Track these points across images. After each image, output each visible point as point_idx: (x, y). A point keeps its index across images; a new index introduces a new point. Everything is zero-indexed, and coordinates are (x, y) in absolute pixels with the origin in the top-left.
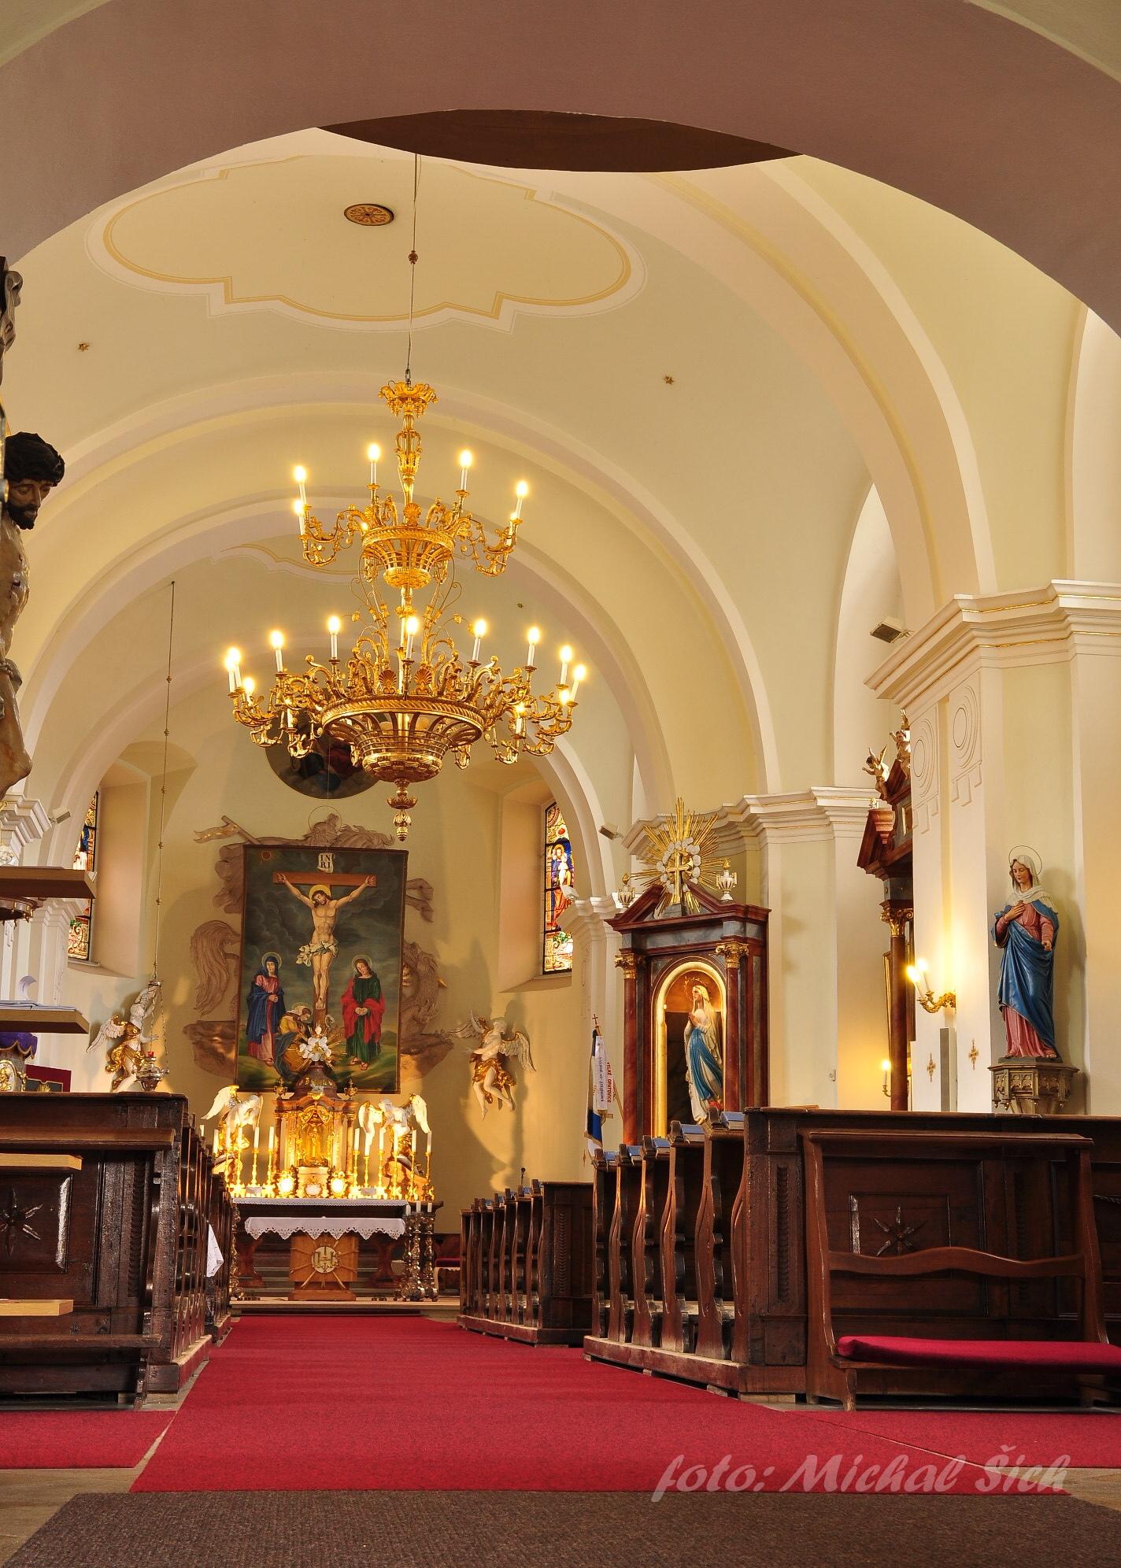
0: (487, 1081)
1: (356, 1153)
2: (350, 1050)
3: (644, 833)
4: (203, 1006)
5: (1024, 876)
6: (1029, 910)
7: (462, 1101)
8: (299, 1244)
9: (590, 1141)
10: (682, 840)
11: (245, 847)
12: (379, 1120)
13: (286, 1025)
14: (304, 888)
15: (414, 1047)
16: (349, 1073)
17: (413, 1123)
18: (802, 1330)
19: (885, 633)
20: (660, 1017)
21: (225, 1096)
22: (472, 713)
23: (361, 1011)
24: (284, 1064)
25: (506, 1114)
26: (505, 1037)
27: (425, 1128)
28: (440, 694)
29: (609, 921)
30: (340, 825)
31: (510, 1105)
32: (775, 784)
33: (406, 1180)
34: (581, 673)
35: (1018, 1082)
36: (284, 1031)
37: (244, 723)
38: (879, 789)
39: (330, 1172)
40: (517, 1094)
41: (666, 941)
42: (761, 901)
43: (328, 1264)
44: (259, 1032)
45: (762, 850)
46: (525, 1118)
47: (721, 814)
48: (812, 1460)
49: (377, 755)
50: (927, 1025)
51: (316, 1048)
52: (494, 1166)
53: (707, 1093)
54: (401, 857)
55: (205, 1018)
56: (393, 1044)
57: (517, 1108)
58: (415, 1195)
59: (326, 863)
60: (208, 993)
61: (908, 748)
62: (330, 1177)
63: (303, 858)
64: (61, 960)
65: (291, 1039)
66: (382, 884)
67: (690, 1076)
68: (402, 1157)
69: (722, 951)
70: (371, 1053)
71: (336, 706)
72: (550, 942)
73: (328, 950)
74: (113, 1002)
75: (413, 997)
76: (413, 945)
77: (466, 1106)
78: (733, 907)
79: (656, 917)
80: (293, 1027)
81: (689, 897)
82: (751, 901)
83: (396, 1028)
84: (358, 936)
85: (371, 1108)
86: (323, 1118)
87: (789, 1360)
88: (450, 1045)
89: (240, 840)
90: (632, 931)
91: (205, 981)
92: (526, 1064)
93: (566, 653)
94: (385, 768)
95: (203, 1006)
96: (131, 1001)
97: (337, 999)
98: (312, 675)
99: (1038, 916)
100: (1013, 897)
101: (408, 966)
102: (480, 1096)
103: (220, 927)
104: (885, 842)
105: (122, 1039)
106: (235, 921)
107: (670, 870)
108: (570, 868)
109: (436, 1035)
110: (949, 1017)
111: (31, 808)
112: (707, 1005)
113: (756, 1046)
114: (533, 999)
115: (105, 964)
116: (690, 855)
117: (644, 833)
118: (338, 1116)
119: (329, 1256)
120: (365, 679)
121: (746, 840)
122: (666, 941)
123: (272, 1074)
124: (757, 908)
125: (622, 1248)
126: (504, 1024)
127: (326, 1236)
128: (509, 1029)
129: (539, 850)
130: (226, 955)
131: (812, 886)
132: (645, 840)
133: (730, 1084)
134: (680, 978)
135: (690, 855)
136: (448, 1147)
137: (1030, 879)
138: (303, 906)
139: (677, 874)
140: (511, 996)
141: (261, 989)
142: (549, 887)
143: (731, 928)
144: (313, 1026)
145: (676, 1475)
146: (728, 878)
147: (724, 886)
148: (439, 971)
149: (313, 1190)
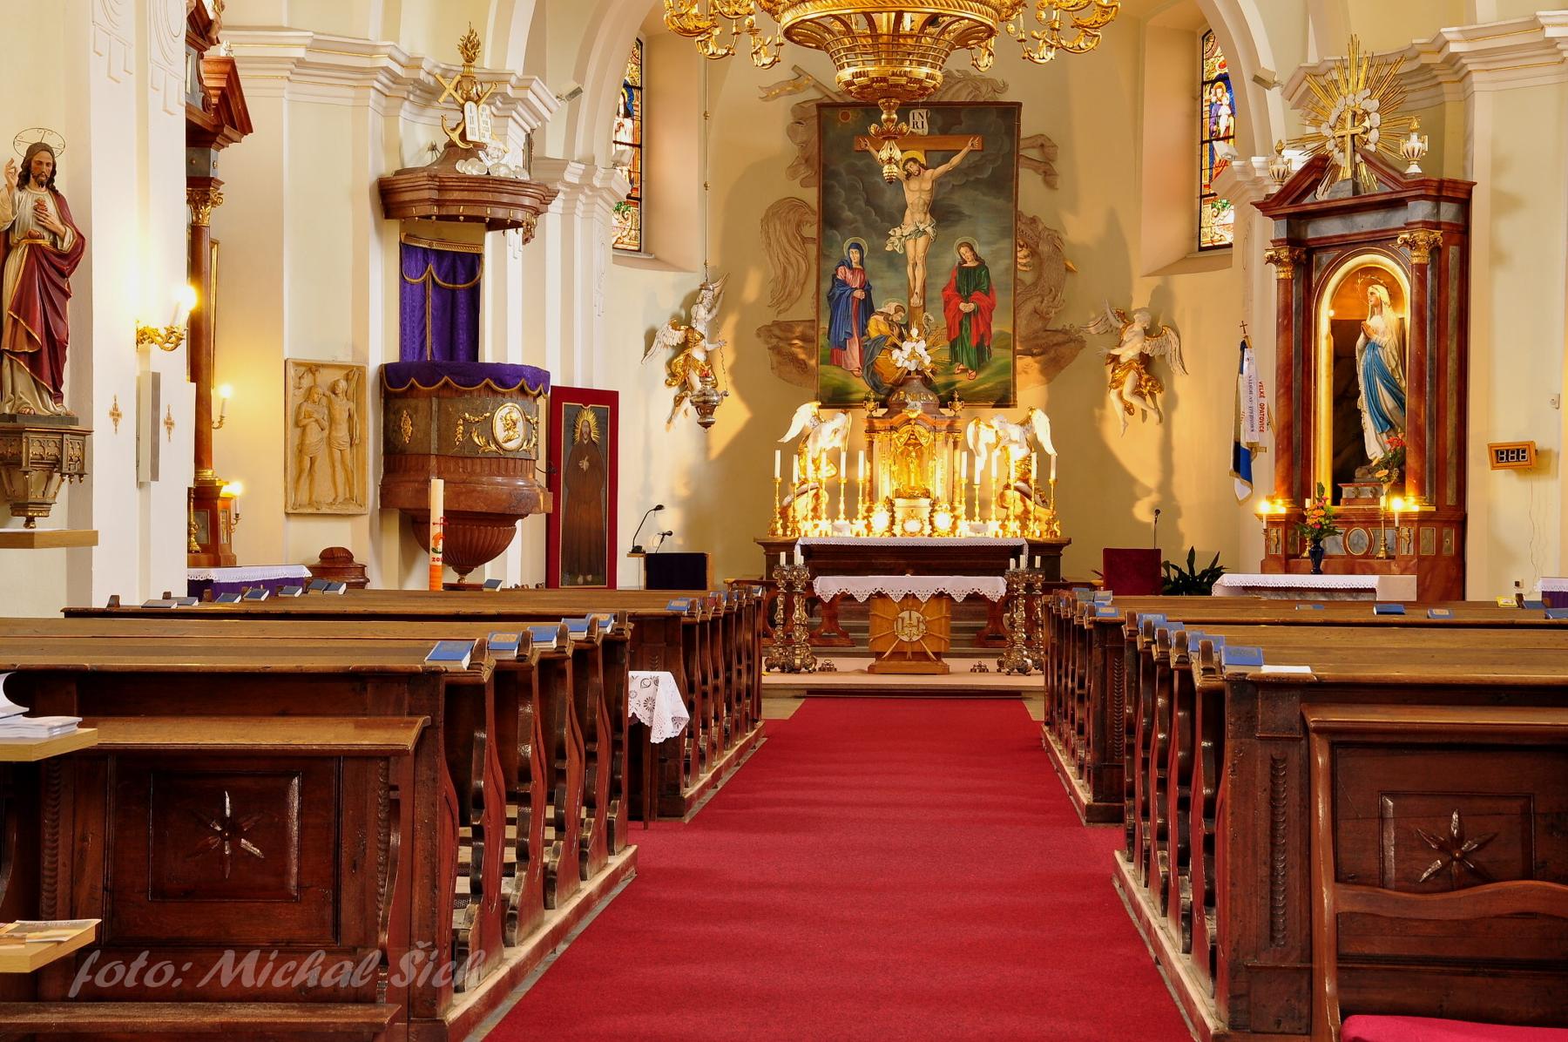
0: (1127, 387)
1: (964, 481)
2: (955, 357)
3: (1305, 85)
7: (1097, 411)
8: (879, 608)
9: (1237, 482)
10: (1356, 95)
11: (821, 106)
12: (993, 440)
13: (876, 326)
15: (1037, 346)
16: (953, 384)
17: (1034, 444)
18: (1305, 985)
20: (1324, 328)
21: (805, 414)
23: (966, 307)
24: (874, 374)
25: (1151, 428)
26: (1148, 333)
27: (1049, 449)
29: (1257, 205)
31: (1156, 417)
33: (1026, 511)
36: (874, 334)
39: (933, 505)
40: (1165, 403)
41: (1331, 228)
42: (1464, 169)
43: (914, 630)
44: (843, 336)
45: (1466, 100)
47: (1410, 54)
48: (229, 955)
51: (913, 354)
52: (1138, 491)
53: (1386, 423)
55: (781, 318)
56: (1006, 347)
57: (1165, 420)
58: (1037, 531)
60: (784, 288)
62: (933, 511)
64: (603, 255)
65: (882, 344)
67: (1363, 403)
69: (1406, 242)
72: (1207, 210)
73: (924, 232)
74: (672, 304)
75: (1035, 284)
76: (1034, 220)
77: (1102, 418)
78: (1421, 183)
80: (884, 328)
81: (1363, 169)
82: (1449, 173)
84: (960, 214)
85: (982, 426)
86: (923, 441)
87: (1285, 1027)
88: (1081, 343)
89: (814, 95)
90: (1289, 216)
91: (779, 272)
92: (1176, 367)
94: (863, 87)
95: (779, 303)
96: (691, 300)
97: (936, 294)
101: (1027, 245)
103: (796, 204)
105: (683, 347)
106: (811, 196)
107: (1338, 133)
108: (1233, 114)
109: (1064, 332)
111: (528, 87)
112: (1387, 310)
113: (1451, 365)
114: (1183, 284)
116: (1367, 113)
117: (1305, 85)
118: (941, 437)
119: (915, 622)
121: (1446, 88)
122: (1331, 228)
123: (861, 387)
124: (1455, 182)
126: (1148, 317)
127: (910, 598)
128: (1153, 324)
129: (1194, 90)
130: (805, 240)
132: (1311, 89)
134: (1367, 270)
135: (1367, 113)
136: (1081, 464)
139: (1348, 139)
140: (1156, 281)
141: (844, 283)
142: (1207, 137)
143: (1420, 210)
144: (908, 327)
145: (93, 971)
146: (1415, 144)
148: (1066, 250)
149: (913, 526)
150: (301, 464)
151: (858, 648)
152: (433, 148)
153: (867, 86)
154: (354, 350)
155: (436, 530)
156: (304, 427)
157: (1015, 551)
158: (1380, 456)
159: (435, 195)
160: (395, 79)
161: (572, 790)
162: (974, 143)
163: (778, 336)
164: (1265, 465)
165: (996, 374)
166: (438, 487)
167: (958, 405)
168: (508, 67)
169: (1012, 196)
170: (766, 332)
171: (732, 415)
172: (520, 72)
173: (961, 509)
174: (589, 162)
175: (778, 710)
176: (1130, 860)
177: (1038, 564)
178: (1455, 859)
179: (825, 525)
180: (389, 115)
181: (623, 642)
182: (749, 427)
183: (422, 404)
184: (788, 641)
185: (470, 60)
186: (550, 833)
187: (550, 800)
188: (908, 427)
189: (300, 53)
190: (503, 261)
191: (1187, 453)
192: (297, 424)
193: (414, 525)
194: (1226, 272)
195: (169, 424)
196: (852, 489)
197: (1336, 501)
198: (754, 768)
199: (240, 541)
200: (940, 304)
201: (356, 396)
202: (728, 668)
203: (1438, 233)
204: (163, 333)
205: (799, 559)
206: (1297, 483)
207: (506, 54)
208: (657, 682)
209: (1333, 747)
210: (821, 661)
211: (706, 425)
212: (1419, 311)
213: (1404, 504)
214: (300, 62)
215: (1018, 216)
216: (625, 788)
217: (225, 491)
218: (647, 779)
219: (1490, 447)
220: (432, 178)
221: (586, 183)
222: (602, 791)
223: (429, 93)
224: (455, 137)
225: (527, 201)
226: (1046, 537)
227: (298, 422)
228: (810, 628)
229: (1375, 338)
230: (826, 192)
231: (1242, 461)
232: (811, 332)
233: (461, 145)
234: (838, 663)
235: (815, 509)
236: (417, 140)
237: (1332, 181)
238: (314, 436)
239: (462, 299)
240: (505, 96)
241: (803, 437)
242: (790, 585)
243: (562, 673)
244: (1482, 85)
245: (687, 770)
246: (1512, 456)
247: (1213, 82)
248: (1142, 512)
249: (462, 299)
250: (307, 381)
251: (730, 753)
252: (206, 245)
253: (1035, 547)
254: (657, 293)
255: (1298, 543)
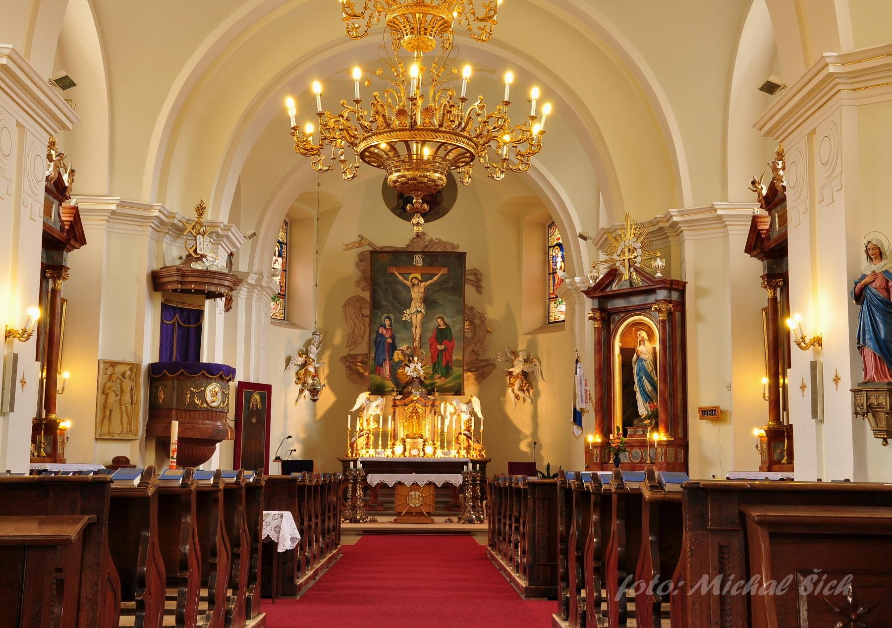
0: (516, 387)
1: (439, 431)
2: (435, 371)
3: (605, 236)
4: (351, 345)
5: (876, 253)
6: (880, 277)
8: (399, 490)
10: (630, 239)
11: (371, 252)
12: (453, 411)
13: (397, 356)
14: (405, 275)
17: (473, 413)
19: (770, 88)
20: (617, 351)
21: (363, 398)
22: (465, 140)
24: (396, 379)
25: (528, 406)
26: (526, 361)
27: (480, 415)
28: (441, 125)
29: (584, 292)
30: (427, 238)
32: (689, 202)
33: (469, 446)
34: (547, 109)
35: (873, 400)
36: (396, 360)
37: (302, 154)
38: (759, 201)
39: (424, 442)
41: (620, 303)
42: (681, 276)
45: (681, 244)
46: (539, 409)
47: (654, 222)
48: (705, 577)
49: (398, 174)
50: (800, 359)
53: (648, 398)
54: (463, 255)
55: (352, 353)
56: (460, 366)
57: (534, 402)
58: (474, 455)
59: (418, 261)
60: (353, 338)
61: (781, 173)
63: (404, 258)
64: (265, 321)
65: (401, 364)
66: (451, 271)
67: (636, 387)
68: (466, 432)
69: (656, 309)
70: (447, 373)
71: (365, 139)
72: (552, 305)
74: (299, 345)
75: (472, 338)
76: (472, 308)
77: (504, 402)
78: (662, 281)
79: (614, 289)
80: (401, 357)
81: (634, 275)
82: (674, 277)
83: (463, 356)
88: (494, 366)
90: (599, 298)
91: (351, 331)
92: (539, 377)
93: (535, 93)
94: (403, 183)
95: (351, 345)
96: (309, 343)
97: (427, 341)
98: (346, 115)
99: (887, 281)
100: (867, 268)
101: (468, 320)
102: (512, 396)
103: (359, 299)
104: (763, 236)
105: (304, 365)
106: (367, 295)
108: (563, 261)
109: (486, 361)
110: (816, 353)
111: (229, 230)
112: (647, 343)
113: (679, 369)
115: (294, 322)
117: (605, 236)
118: (428, 409)
120: (384, 116)
121: (671, 239)
123: (390, 385)
124: (678, 281)
125: (578, 557)
126: (526, 354)
127: (415, 485)
129: (545, 251)
131: (718, 271)
132: (606, 240)
133: (662, 393)
136: (494, 426)
137: (880, 255)
138: (405, 286)
139: (626, 261)
140: (529, 337)
141: (382, 335)
143: (662, 294)
144: (413, 356)
146: (659, 263)
147: (657, 268)
148: (487, 323)
149: (414, 452)
150: (104, 412)
151: (387, 512)
152: (181, 258)
153: (406, 183)
154: (135, 355)
155: (174, 447)
156: (107, 394)
157: (466, 463)
158: (645, 413)
159: (180, 279)
160: (162, 223)
161: (221, 576)
162: (444, 271)
163: (350, 361)
164: (590, 418)
165: (455, 379)
166: (175, 424)
167: (437, 394)
168: (220, 220)
169: (463, 296)
170: (344, 359)
171: (327, 398)
172: (226, 222)
173: (438, 444)
174: (260, 274)
175: (349, 541)
176: (566, 619)
177: (478, 468)
178: (851, 620)
179: (372, 452)
180: (159, 241)
181: (260, 487)
182: (335, 403)
183: (169, 383)
184: (354, 508)
185: (200, 215)
186: (203, 606)
187: (204, 585)
188: (412, 404)
189: (114, 207)
190: (213, 314)
191: (551, 422)
192: (103, 393)
193: (163, 446)
194: (562, 332)
195: (23, 382)
196: (385, 435)
197: (625, 435)
198: (335, 569)
199: (69, 451)
200: (428, 346)
201: (135, 378)
202: (323, 514)
203: (671, 306)
204: (20, 332)
205: (360, 466)
206: (605, 428)
207: (219, 213)
208: (282, 516)
209: (772, 535)
210: (369, 518)
211: (315, 401)
212: (663, 342)
213: (659, 436)
214: (113, 212)
215: (465, 306)
216: (259, 578)
217: (62, 425)
218: (273, 573)
219: (699, 409)
220: (178, 270)
221: (258, 285)
222: (242, 577)
223: (178, 231)
224: (192, 252)
225: (227, 283)
226: (479, 458)
227: (104, 391)
228: (365, 501)
229: (642, 356)
230: (374, 293)
231: (577, 417)
232: (366, 360)
233: (194, 255)
234: (378, 518)
235: (367, 444)
236: (173, 253)
237: (620, 281)
238: (112, 398)
239: (192, 333)
240: (217, 233)
241: (362, 409)
242: (355, 479)
243: (216, 500)
244: (689, 237)
245: (299, 569)
246: (711, 413)
247: (554, 247)
248: (524, 446)
249: (192, 333)
250: (110, 371)
251: (324, 561)
252: (58, 301)
253: (474, 462)
254: (293, 339)
255: (606, 454)
